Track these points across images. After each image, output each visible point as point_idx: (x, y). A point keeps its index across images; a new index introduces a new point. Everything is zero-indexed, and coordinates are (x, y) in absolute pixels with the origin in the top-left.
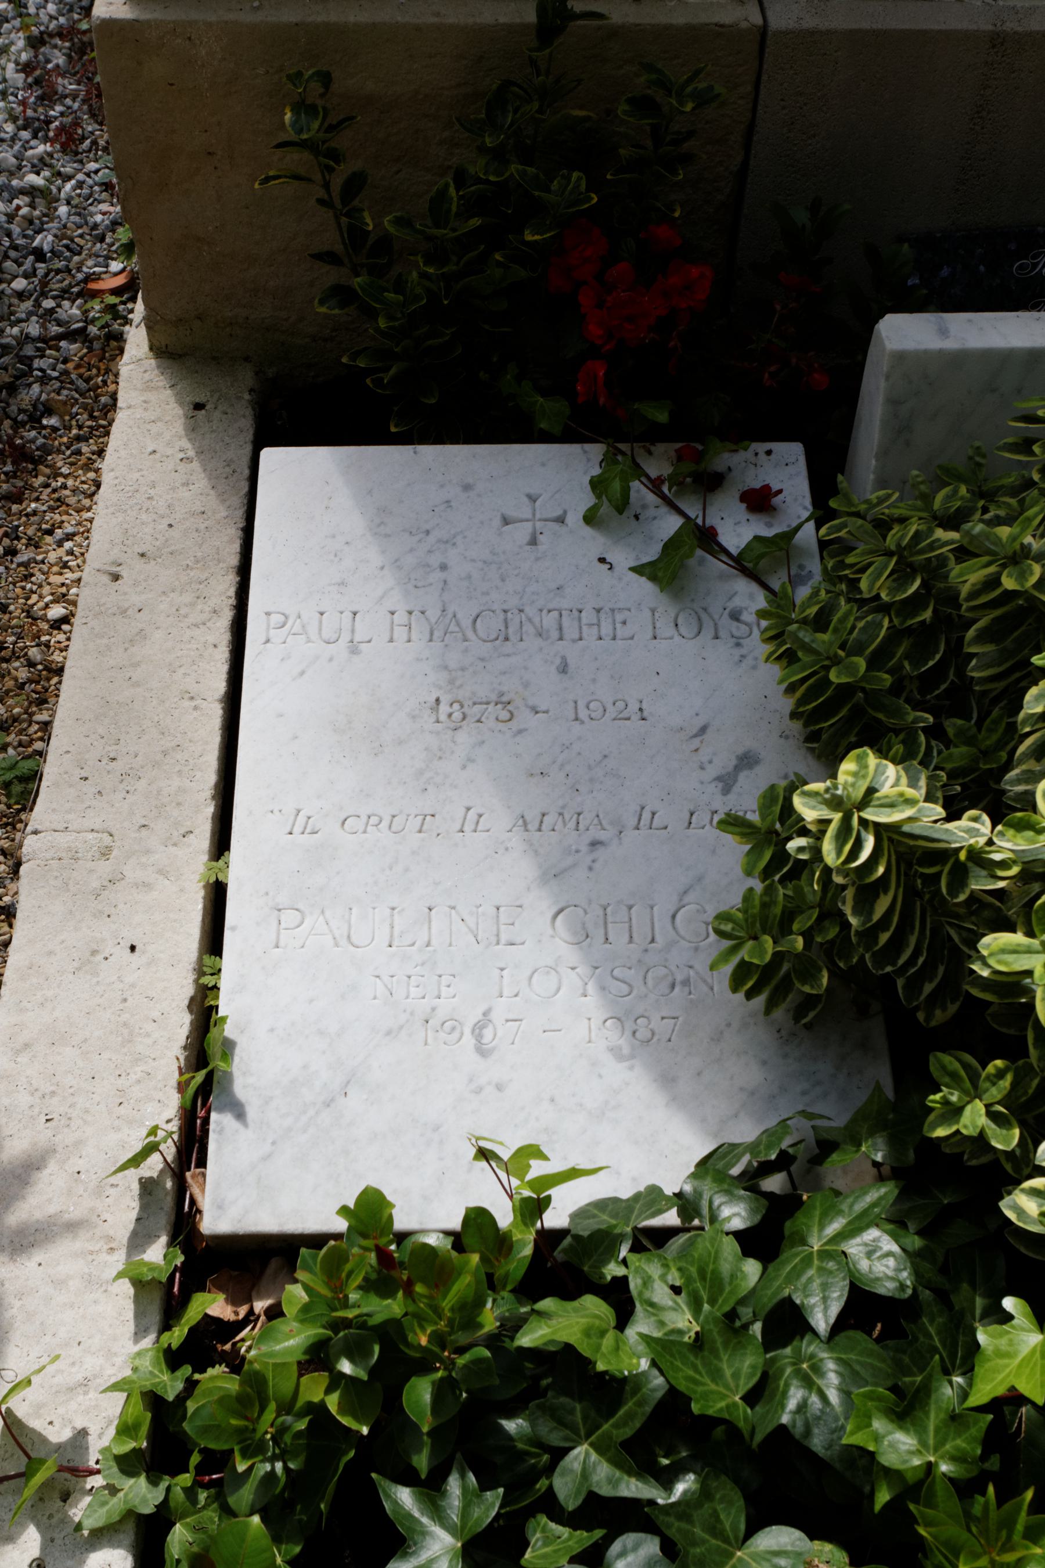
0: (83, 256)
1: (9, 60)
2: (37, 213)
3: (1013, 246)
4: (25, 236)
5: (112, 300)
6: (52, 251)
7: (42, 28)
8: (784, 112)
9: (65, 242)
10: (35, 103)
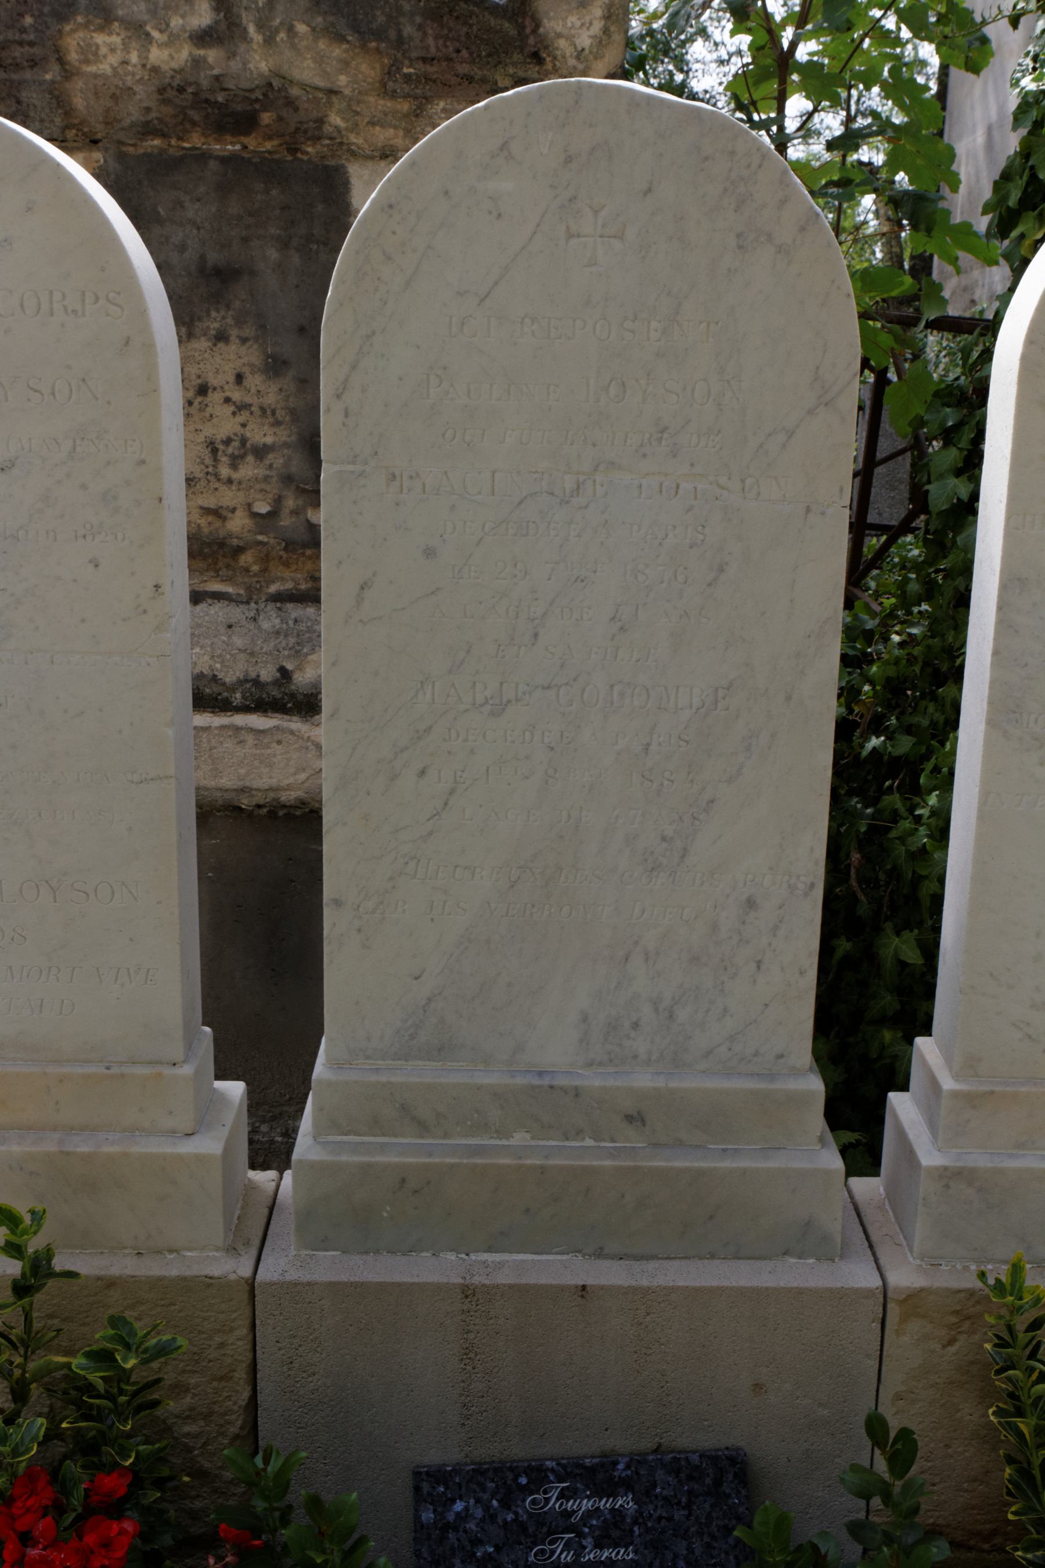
3: (523, 1480)
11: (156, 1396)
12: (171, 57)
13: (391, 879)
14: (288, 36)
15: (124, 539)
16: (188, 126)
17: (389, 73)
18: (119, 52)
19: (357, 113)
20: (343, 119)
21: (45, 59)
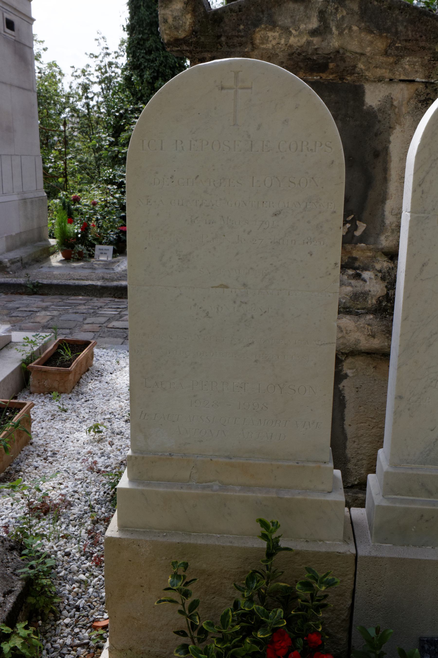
0: (94, 610)
1: (84, 529)
2: (81, 590)
4: (74, 600)
5: (101, 632)
6: (83, 608)
7: (98, 517)
8: (367, 586)
9: (89, 604)
10: (89, 546)
11: (325, 602)
12: (299, 41)
13: (425, 388)
14: (349, 32)
15: (324, 244)
16: (298, 69)
17: (389, 46)
18: (277, 39)
19: (370, 63)
20: (364, 65)
21: (246, 43)
